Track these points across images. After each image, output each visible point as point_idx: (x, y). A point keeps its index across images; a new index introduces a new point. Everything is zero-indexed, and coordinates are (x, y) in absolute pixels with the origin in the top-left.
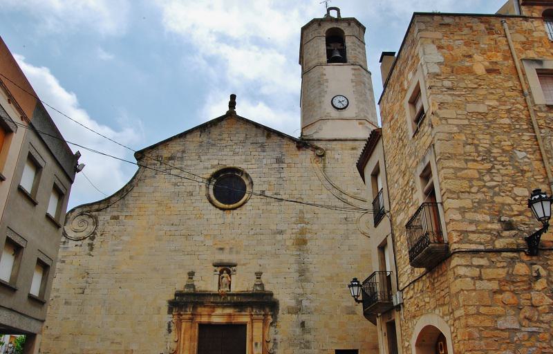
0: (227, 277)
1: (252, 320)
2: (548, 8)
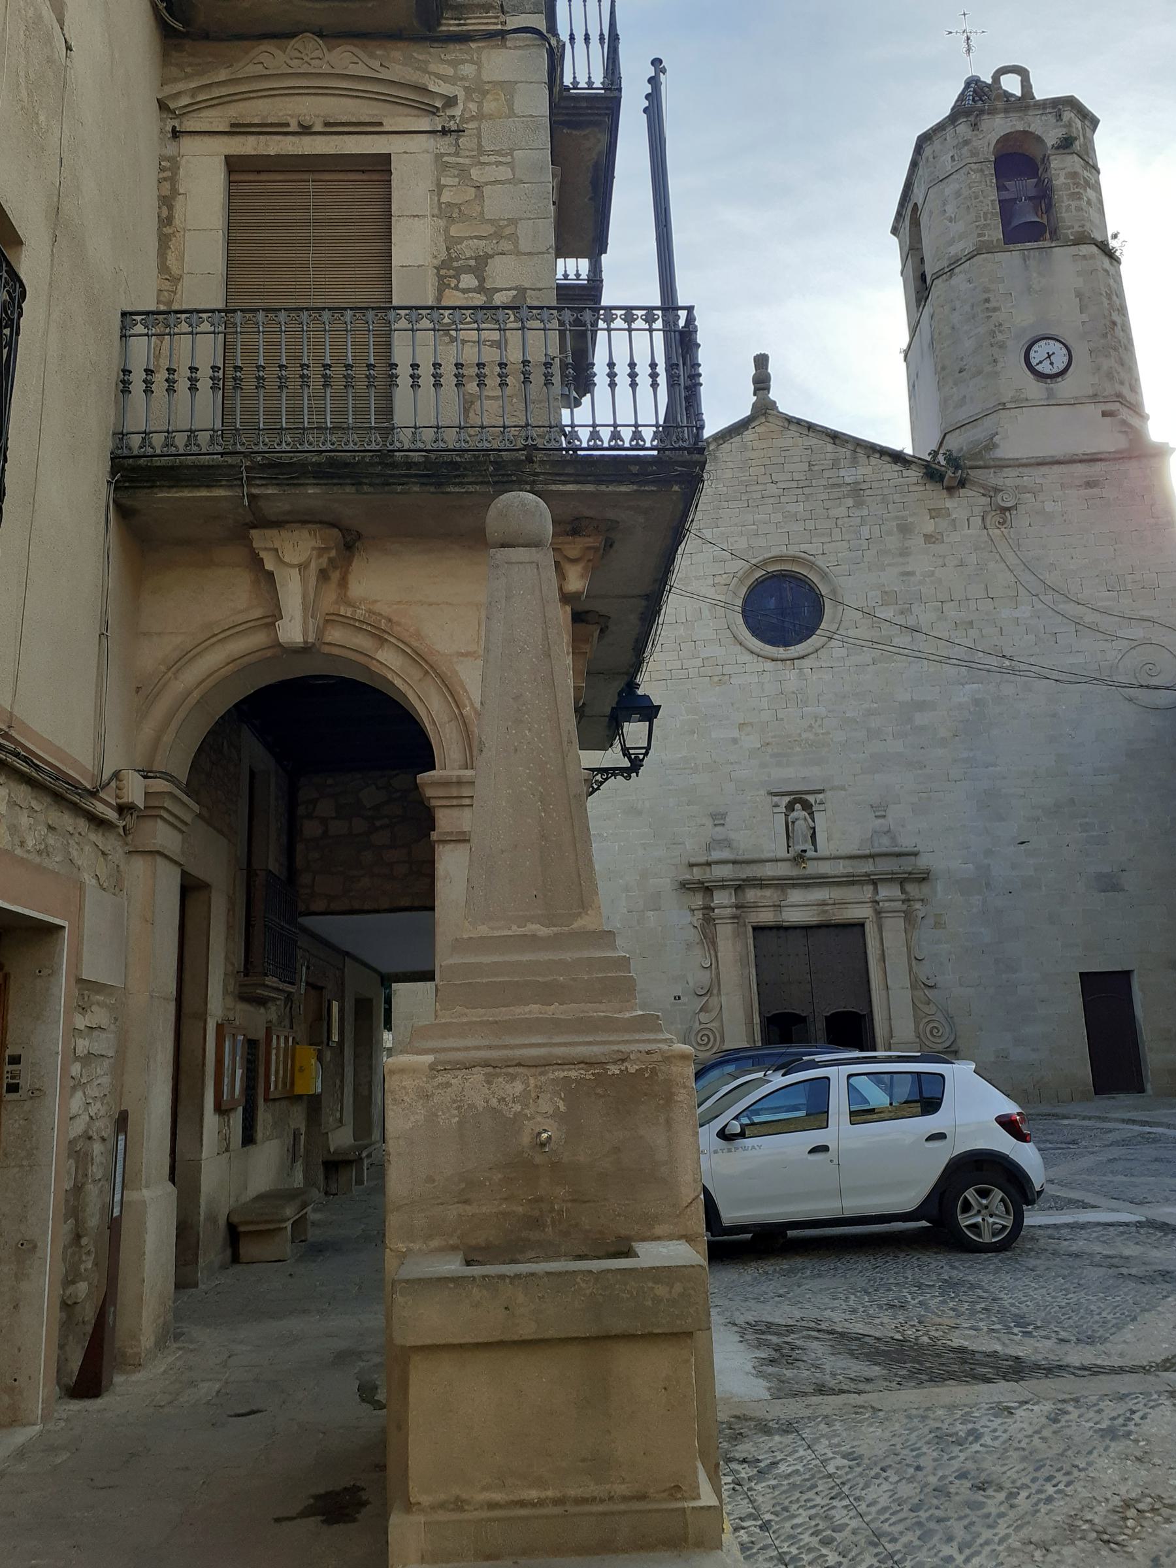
0: (805, 819)
1: (878, 913)
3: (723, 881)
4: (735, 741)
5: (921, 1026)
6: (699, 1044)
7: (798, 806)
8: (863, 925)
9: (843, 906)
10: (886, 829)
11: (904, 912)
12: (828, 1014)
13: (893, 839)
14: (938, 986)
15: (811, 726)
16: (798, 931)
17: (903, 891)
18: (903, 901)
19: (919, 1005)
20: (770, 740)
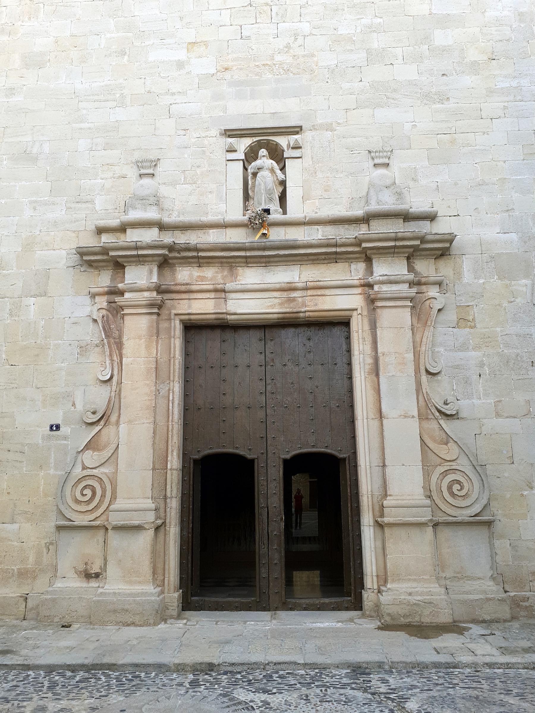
0: (272, 171)
1: (371, 301)
2: (255, 139)
3: (137, 248)
4: (180, 65)
5: (434, 479)
6: (77, 502)
7: (263, 152)
8: (346, 323)
9: (319, 292)
10: (388, 182)
11: (412, 299)
12: (288, 456)
13: (399, 195)
14: (461, 415)
15: (288, 46)
16: (252, 332)
17: (411, 269)
18: (412, 284)
19: (431, 445)
20: (230, 64)
